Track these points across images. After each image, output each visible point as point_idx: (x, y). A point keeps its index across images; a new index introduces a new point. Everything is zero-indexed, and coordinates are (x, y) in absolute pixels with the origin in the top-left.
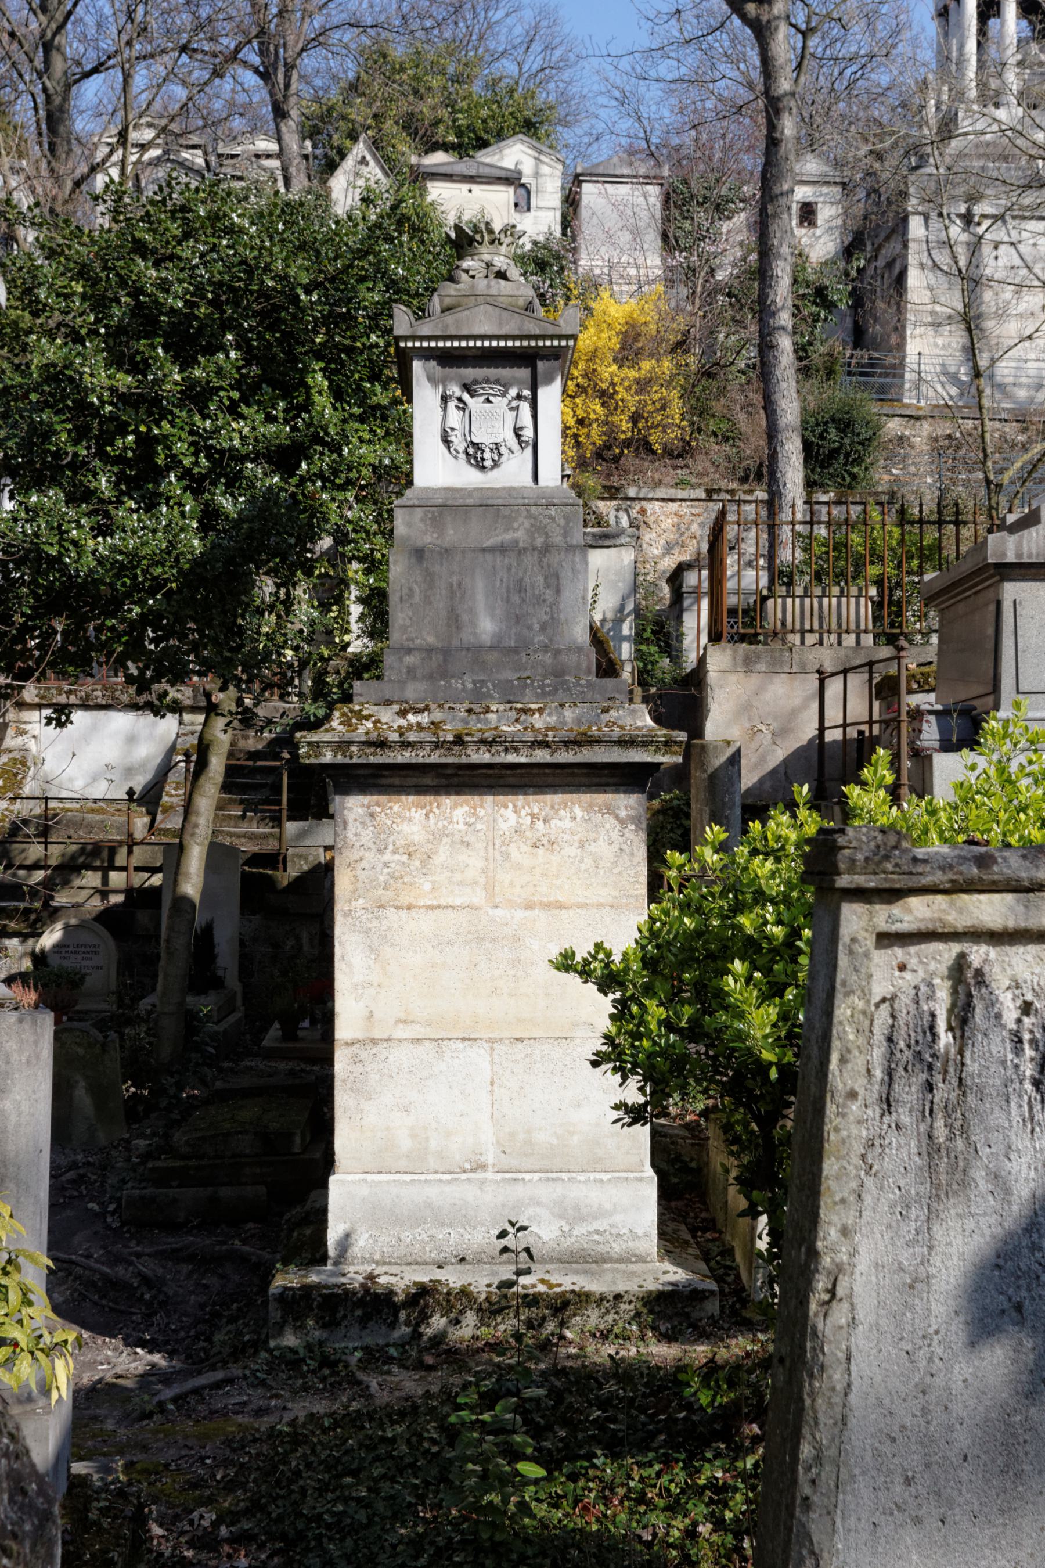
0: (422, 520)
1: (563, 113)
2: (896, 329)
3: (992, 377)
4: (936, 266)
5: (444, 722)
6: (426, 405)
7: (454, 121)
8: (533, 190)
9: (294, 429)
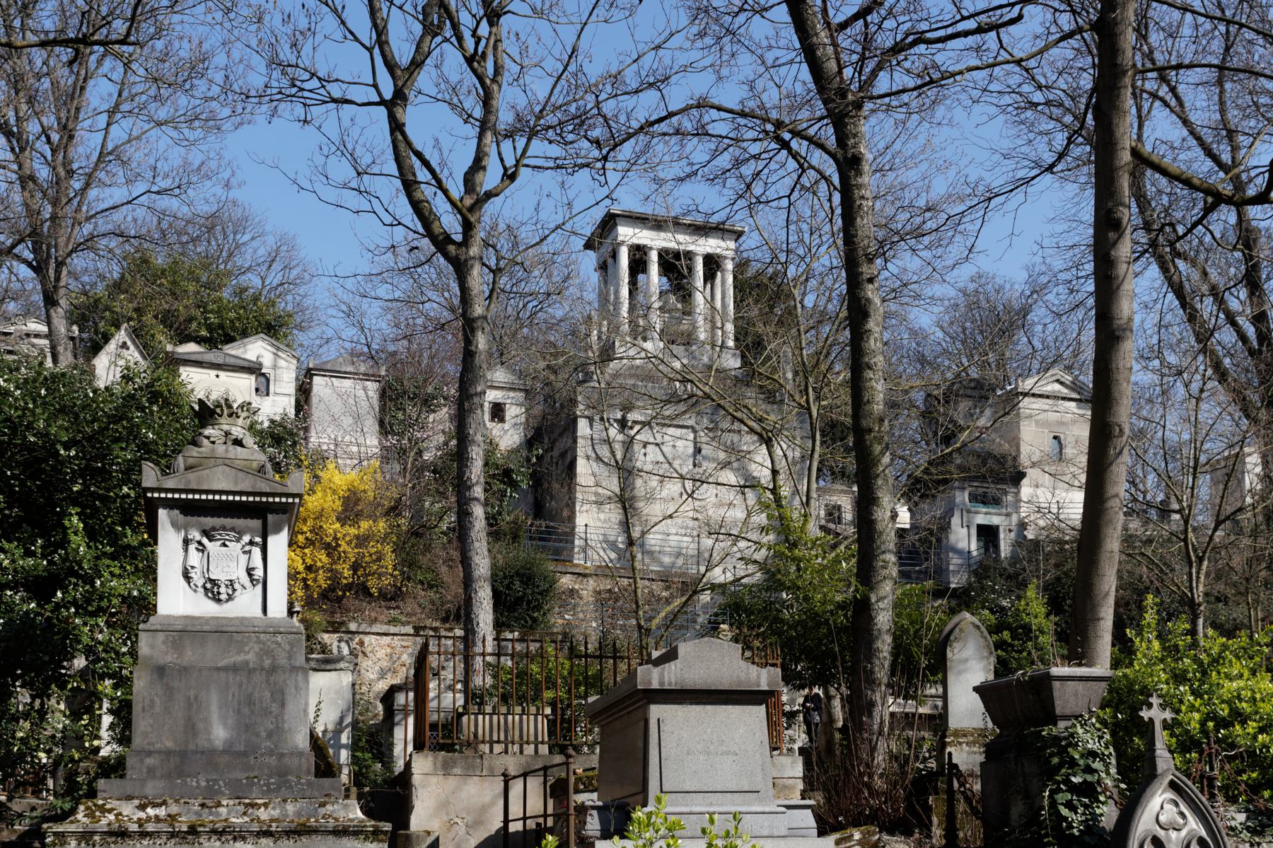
0: (164, 642)
1: (298, 320)
2: (568, 505)
3: (642, 545)
4: (599, 459)
5: (179, 815)
6: (170, 546)
7: (206, 319)
8: (272, 378)
9: (51, 563)
